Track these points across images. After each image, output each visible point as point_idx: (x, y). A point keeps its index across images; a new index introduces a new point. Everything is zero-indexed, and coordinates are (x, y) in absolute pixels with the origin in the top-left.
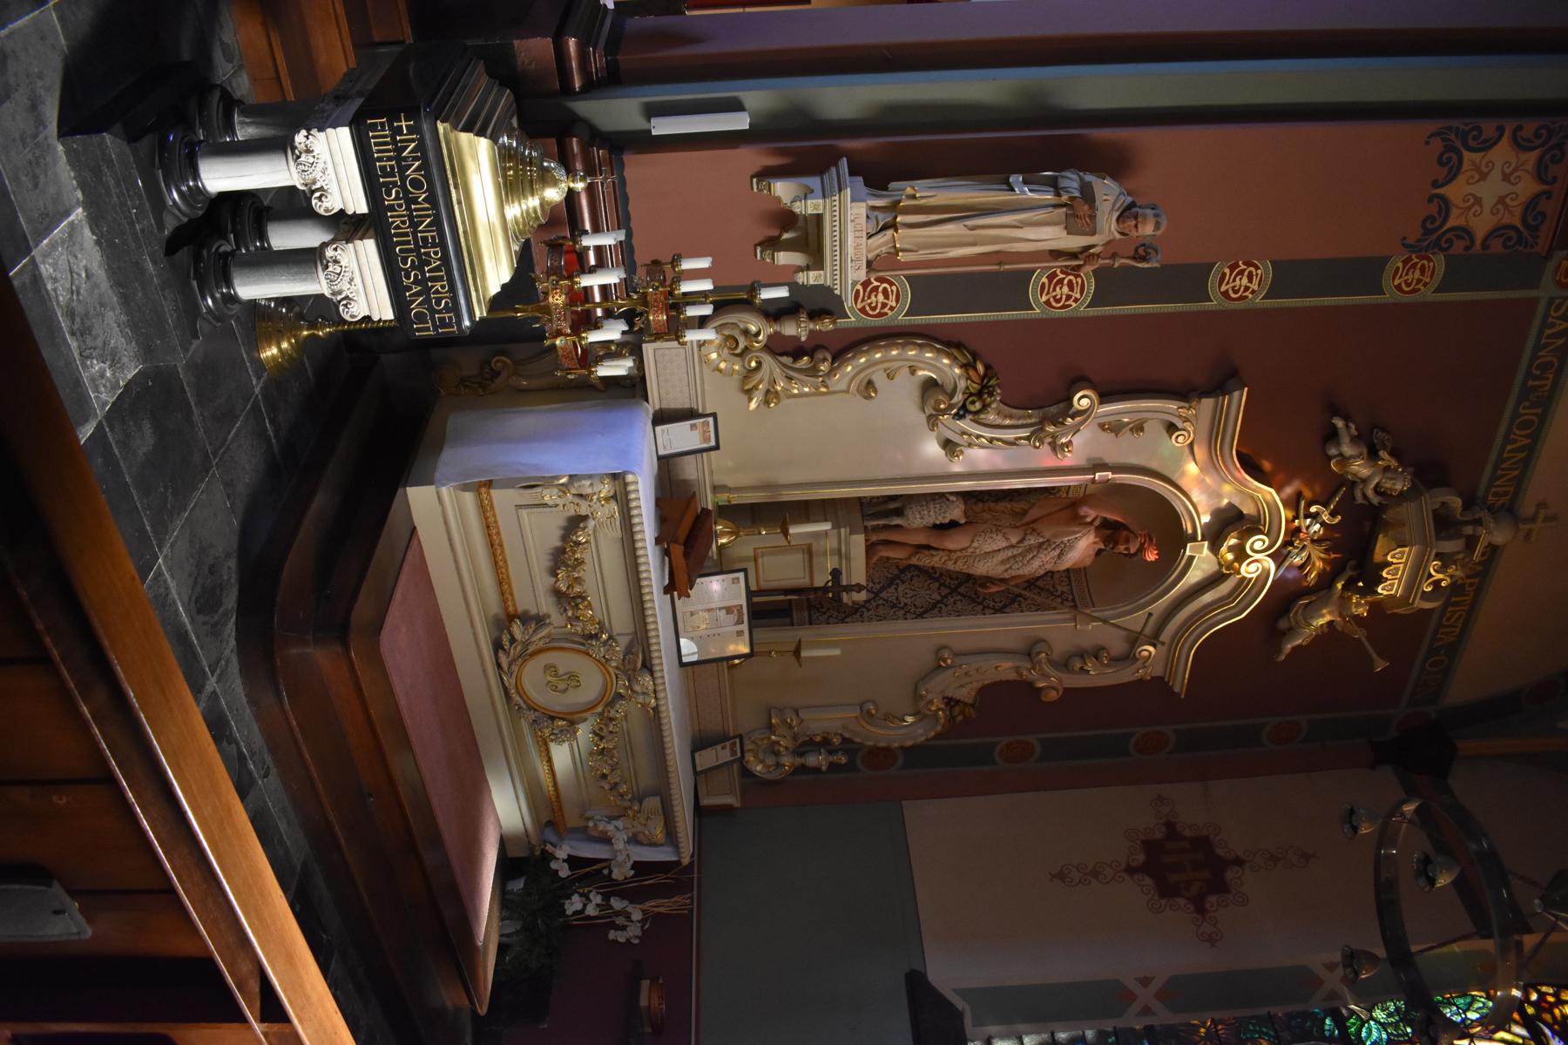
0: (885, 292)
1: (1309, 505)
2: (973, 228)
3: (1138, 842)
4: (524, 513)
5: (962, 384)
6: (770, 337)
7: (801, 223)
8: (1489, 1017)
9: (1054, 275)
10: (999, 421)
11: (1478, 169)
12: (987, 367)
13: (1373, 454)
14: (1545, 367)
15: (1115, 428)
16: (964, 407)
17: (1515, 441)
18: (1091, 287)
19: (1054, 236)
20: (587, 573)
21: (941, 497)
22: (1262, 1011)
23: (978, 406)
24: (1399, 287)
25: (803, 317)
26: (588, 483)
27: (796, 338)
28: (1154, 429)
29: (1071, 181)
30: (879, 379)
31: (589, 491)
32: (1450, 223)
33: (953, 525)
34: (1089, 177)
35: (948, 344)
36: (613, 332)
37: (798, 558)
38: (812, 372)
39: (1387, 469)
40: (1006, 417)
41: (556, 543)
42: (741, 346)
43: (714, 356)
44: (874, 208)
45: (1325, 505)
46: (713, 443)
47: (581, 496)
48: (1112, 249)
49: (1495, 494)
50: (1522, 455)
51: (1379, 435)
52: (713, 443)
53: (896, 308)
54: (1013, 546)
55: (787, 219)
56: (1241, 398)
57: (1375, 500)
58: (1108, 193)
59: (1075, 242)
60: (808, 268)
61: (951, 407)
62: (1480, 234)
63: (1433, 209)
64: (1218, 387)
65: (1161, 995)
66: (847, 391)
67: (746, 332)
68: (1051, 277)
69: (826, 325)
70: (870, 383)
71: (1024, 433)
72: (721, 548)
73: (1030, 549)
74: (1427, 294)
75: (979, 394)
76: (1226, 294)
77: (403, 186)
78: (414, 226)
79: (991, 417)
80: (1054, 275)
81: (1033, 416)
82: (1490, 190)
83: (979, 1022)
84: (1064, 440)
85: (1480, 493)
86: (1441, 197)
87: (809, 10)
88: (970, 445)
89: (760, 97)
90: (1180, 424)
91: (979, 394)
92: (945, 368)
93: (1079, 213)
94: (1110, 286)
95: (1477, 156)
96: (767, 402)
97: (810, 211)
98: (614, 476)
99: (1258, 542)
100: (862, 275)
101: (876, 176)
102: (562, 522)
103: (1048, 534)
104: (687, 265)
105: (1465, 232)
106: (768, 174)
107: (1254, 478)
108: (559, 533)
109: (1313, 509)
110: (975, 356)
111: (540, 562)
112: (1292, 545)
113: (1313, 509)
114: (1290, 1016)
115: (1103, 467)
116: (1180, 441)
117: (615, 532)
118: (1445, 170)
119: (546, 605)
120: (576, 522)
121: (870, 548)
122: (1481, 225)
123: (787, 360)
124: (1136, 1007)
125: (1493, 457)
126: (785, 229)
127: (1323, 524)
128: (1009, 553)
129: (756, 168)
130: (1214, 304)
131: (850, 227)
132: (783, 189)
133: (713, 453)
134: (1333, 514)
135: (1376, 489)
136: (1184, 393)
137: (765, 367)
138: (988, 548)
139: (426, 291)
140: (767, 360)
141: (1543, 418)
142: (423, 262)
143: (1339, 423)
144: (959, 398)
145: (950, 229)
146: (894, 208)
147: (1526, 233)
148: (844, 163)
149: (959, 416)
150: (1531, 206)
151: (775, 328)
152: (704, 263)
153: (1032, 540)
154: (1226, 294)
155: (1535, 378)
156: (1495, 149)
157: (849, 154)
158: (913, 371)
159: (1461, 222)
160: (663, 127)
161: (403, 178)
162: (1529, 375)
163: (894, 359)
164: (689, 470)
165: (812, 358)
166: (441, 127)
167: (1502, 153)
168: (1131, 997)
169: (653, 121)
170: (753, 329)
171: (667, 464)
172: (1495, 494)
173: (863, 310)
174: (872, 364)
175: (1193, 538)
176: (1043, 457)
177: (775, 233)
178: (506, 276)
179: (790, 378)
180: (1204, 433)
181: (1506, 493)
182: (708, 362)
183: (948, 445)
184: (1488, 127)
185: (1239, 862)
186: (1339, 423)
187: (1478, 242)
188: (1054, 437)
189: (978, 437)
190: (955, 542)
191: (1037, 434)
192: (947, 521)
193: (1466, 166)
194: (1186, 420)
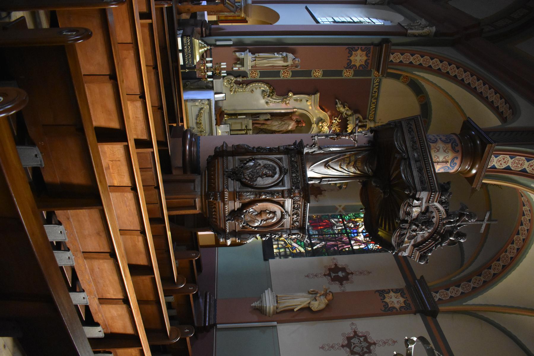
0: (255, 73)
1: (334, 117)
2: (268, 61)
3: (373, 353)
4: (192, 107)
5: (269, 91)
6: (235, 81)
7: (241, 60)
9: (284, 71)
10: (276, 98)
11: (355, 55)
12: (273, 88)
13: (344, 107)
14: (375, 92)
15: (296, 100)
16: (269, 95)
17: (372, 106)
18: (291, 74)
19: (281, 63)
20: (202, 119)
21: (266, 113)
22: (327, 214)
23: (271, 95)
24: (346, 76)
25: (241, 77)
26: (204, 101)
27: (240, 81)
28: (304, 101)
29: (284, 54)
30: (254, 89)
31: (204, 102)
32: (352, 64)
33: (268, 120)
34: (287, 53)
35: (266, 83)
36: (210, 73)
37: (240, 125)
38: (242, 87)
39: (347, 110)
40: (277, 97)
41: (197, 113)
42: (230, 82)
43: (225, 84)
44: (252, 57)
45: (338, 118)
46: (225, 99)
47: (202, 104)
48: (292, 66)
49: (370, 117)
50: (374, 109)
51: (346, 104)
52: (225, 99)
53: (257, 77)
54: (279, 124)
55: (238, 59)
56: (318, 95)
57: (346, 116)
58: (291, 56)
59: (285, 64)
60: (242, 67)
61: (267, 95)
62: (358, 67)
63: (349, 61)
64: (314, 93)
66: (249, 91)
67: (231, 80)
68: (284, 72)
69: (245, 79)
70: (253, 90)
71: (280, 101)
72: (225, 120)
73: (283, 125)
74: (351, 77)
75: (272, 93)
76: (315, 76)
77: (187, 46)
78: (188, 51)
79: (274, 97)
80: (284, 71)
81: (282, 98)
82: (358, 58)
84: (288, 102)
85: (367, 116)
86: (350, 59)
87: (280, 80)
88: (271, 103)
89: (234, 38)
90: (308, 100)
91: (272, 93)
92: (265, 87)
93: (285, 59)
94: (294, 73)
95: (355, 52)
96: (234, 93)
97: (242, 57)
98: (208, 100)
99: (324, 124)
100: (250, 68)
102: (199, 109)
103: (286, 121)
104: (222, 64)
105: (355, 65)
106: (235, 51)
108: (198, 111)
109: (335, 118)
110: (271, 86)
111: (194, 117)
112: (332, 126)
113: (335, 118)
114: (332, 215)
115: (295, 108)
116: (309, 103)
117: (208, 111)
118: (368, 62)
119: (195, 126)
120: (202, 109)
121: (253, 124)
122: (358, 64)
123: (238, 85)
125: (368, 110)
126: (238, 61)
127: (338, 122)
128: (279, 125)
129: (233, 51)
130: (313, 78)
131: (248, 60)
132: (238, 54)
133: (224, 101)
134: (339, 120)
135: (346, 114)
136: (308, 94)
137: (234, 86)
138: (275, 124)
139: (188, 60)
140: (234, 84)
141: (377, 102)
142: (189, 56)
143: (337, 101)
144: (268, 93)
145: (265, 61)
146: (256, 57)
147: (366, 66)
148: (248, 50)
149: (268, 97)
150: (366, 61)
152: (225, 64)
153: (283, 123)
154: (315, 76)
155: (374, 94)
156: (358, 51)
157: (248, 49)
158: (260, 88)
159: (354, 64)
160: (218, 43)
161: (187, 45)
162: (372, 93)
163: (256, 86)
164: (220, 104)
165: (242, 85)
166: (193, 38)
167: (359, 52)
169: (217, 42)
170: (232, 79)
171: (217, 102)
172: (370, 117)
173: (251, 77)
174: (253, 86)
175: (313, 124)
176: (283, 105)
177: (236, 62)
178: (199, 60)
179: (238, 88)
180: (313, 101)
181: (372, 117)
182: (224, 85)
183: (267, 103)
184: (356, 47)
185: (325, 190)
186: (337, 101)
187: (358, 68)
188: (285, 101)
189: (272, 101)
190: (269, 122)
191: (282, 101)
192: (267, 119)
194: (309, 99)
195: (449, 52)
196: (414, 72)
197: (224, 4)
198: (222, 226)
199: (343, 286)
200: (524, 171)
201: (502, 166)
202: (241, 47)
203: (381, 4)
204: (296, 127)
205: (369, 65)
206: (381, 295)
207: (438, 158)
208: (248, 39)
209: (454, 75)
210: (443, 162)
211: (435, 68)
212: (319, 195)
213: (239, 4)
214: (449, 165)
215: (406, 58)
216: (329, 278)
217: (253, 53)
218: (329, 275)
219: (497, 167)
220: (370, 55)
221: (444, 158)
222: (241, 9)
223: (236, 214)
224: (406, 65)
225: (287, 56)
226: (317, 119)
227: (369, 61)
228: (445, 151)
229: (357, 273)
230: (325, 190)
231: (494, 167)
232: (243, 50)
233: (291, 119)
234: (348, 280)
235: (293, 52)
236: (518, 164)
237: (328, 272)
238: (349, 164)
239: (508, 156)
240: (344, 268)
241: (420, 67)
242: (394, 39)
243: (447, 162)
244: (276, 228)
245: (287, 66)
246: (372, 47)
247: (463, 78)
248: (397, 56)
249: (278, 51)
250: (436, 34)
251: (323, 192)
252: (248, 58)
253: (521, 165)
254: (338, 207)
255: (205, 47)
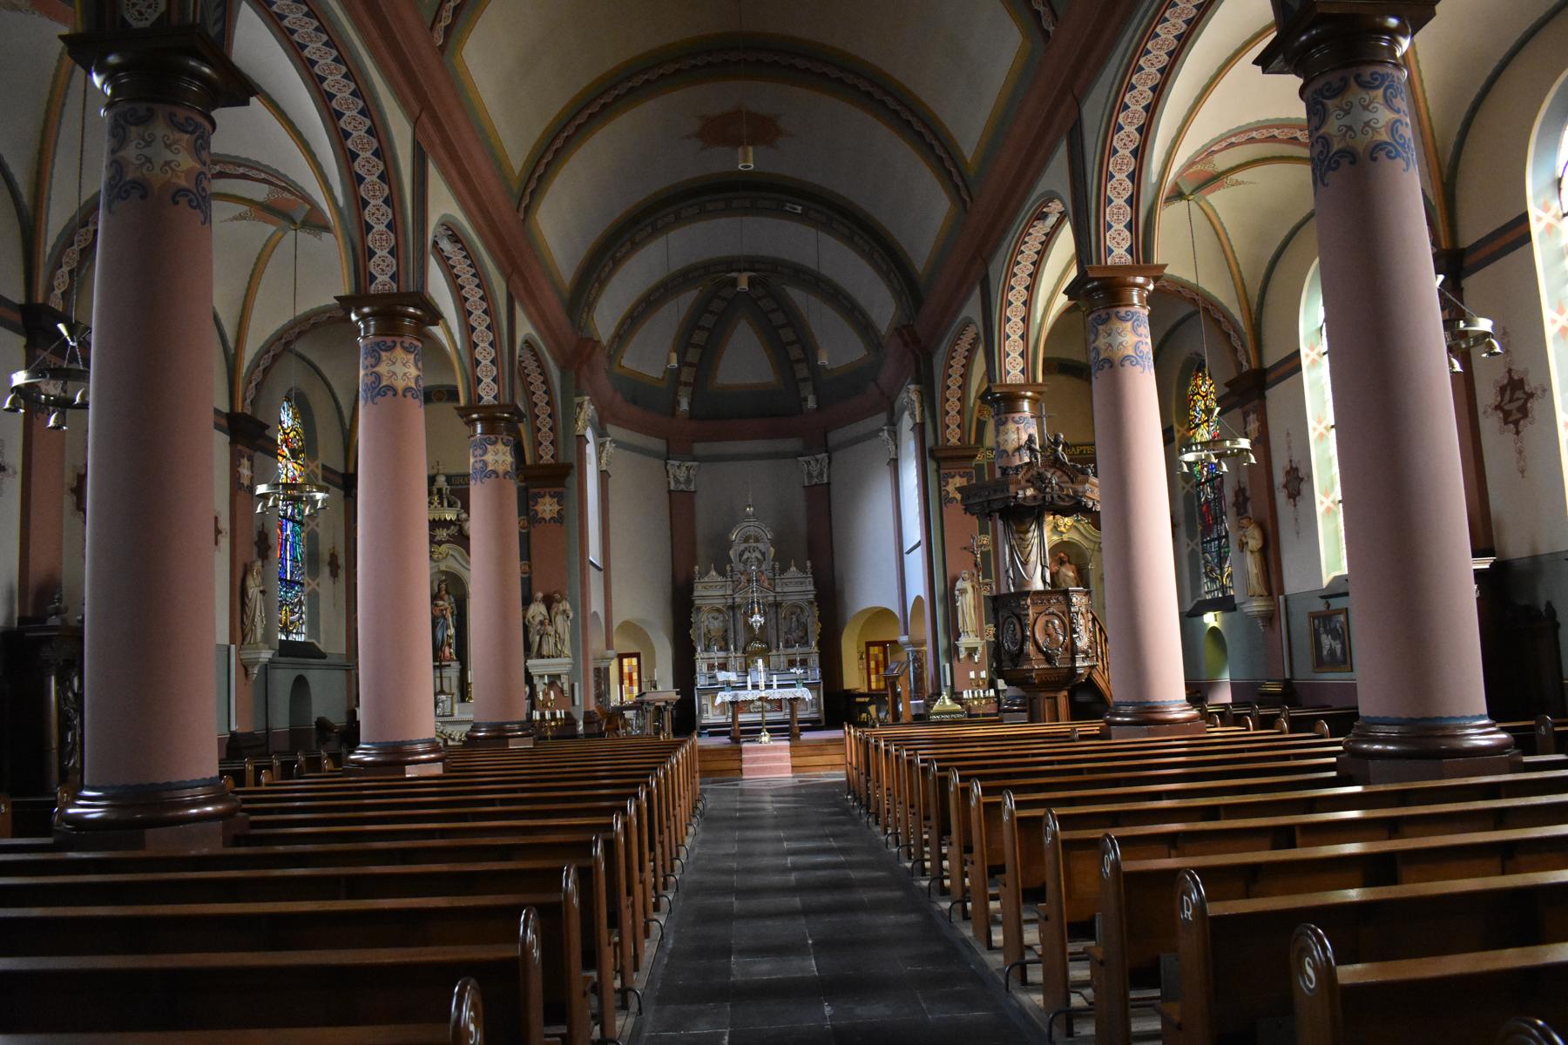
8: (1177, 452)
29: (957, 593)
32: (1101, 357)
58: (959, 585)
59: (970, 590)
65: (1192, 541)
83: (1200, 596)
93: (964, 591)
101: (958, 636)
103: (1061, 581)
106: (959, 659)
107: (1327, 336)
124: (1195, 547)
132: (961, 656)
151: (55, 786)
160: (949, 683)
168: (1193, 550)
184: (943, 493)
185: (1510, 371)
193: (1101, 331)
195: (938, 361)
196: (972, 405)
197: (899, 676)
198: (1066, 671)
199: (1534, 392)
200: (1022, 337)
201: (146, 19)
202: (952, 652)
203: (896, 436)
204: (1070, 563)
205: (967, 470)
206: (1334, 166)
207: (1014, 440)
208: (943, 643)
209: (1012, 300)
210: (1018, 433)
211: (1138, 140)
212: (1526, 388)
213: (910, 655)
214: (1022, 425)
215: (1015, 346)
216: (1522, 422)
217: (959, 635)
218: (1516, 423)
219: (1022, 367)
220: (952, 471)
221: (1013, 432)
222: (918, 652)
223: (1049, 658)
224: (962, 419)
225: (958, 590)
226: (1054, 534)
227: (962, 471)
228: (1006, 433)
229: (1508, 359)
230: (1510, 371)
231: (1130, 251)
232: (957, 649)
233: (1057, 573)
234: (1522, 379)
235: (955, 580)
236: (1015, 346)
237: (1512, 426)
238: (1023, 540)
239: (1007, 360)
240: (1501, 388)
241: (962, 400)
242: (930, 442)
243: (1018, 429)
244: (1067, 622)
245: (973, 587)
246: (942, 471)
247: (1157, 70)
248: (1114, 238)
249: (954, 601)
250: (917, 381)
251: (1516, 378)
252: (965, 641)
253: (1119, 208)
254: (1185, 490)
255: (944, 698)
